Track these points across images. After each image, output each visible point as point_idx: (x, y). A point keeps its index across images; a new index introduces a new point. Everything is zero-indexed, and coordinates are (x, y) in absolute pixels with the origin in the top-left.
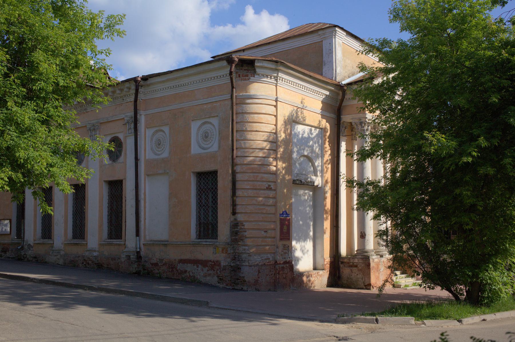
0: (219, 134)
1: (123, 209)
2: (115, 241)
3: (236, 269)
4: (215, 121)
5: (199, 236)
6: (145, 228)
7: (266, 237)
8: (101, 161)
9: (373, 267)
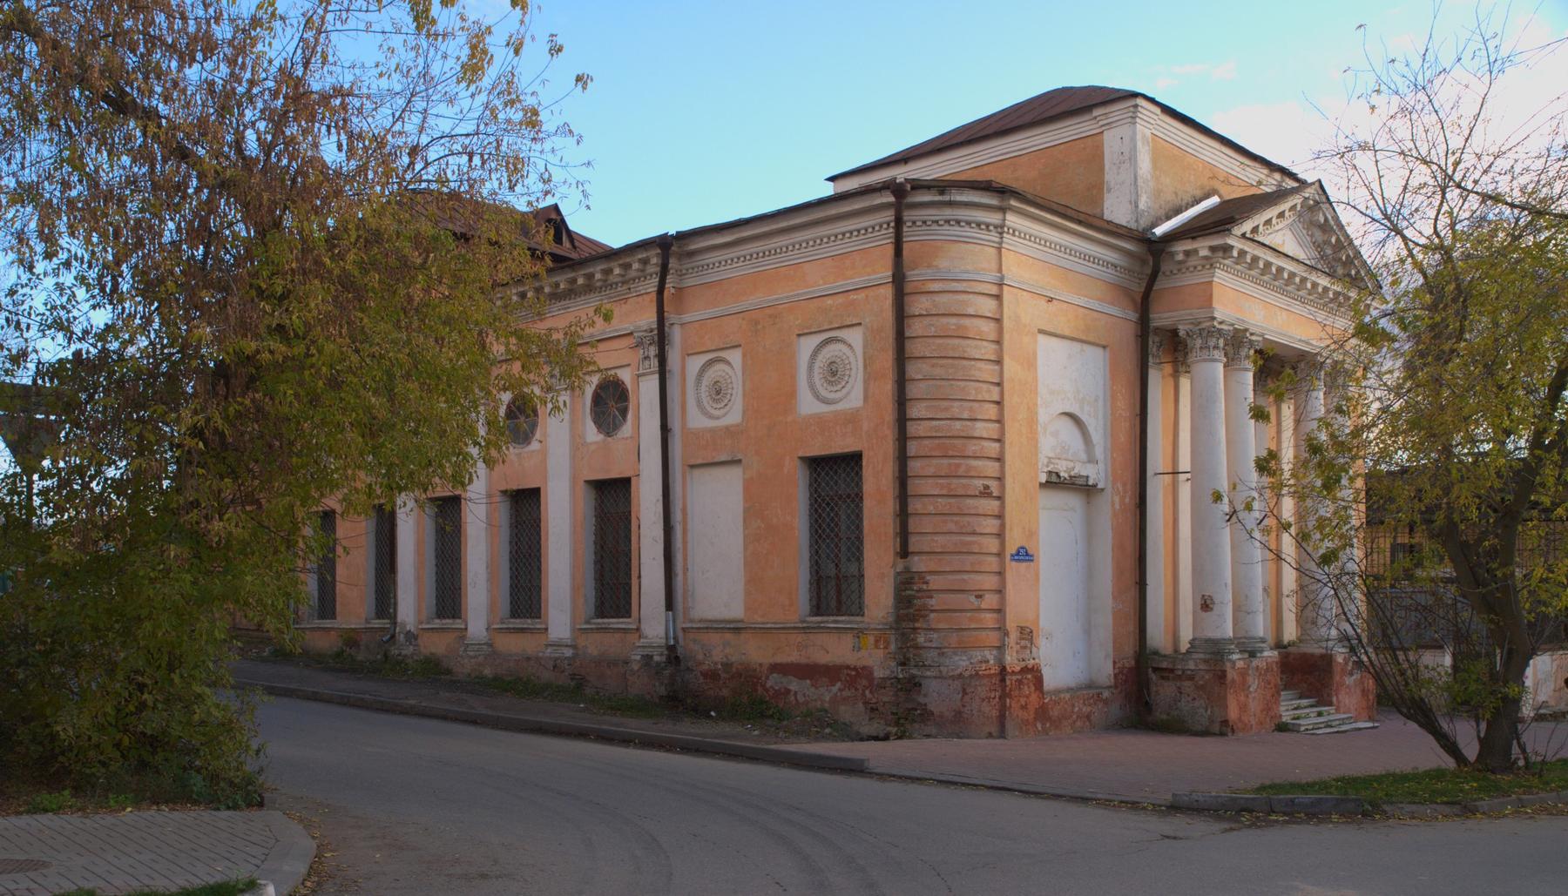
0: (865, 367)
2: (614, 622)
3: (912, 686)
4: (855, 337)
9: (1233, 681)
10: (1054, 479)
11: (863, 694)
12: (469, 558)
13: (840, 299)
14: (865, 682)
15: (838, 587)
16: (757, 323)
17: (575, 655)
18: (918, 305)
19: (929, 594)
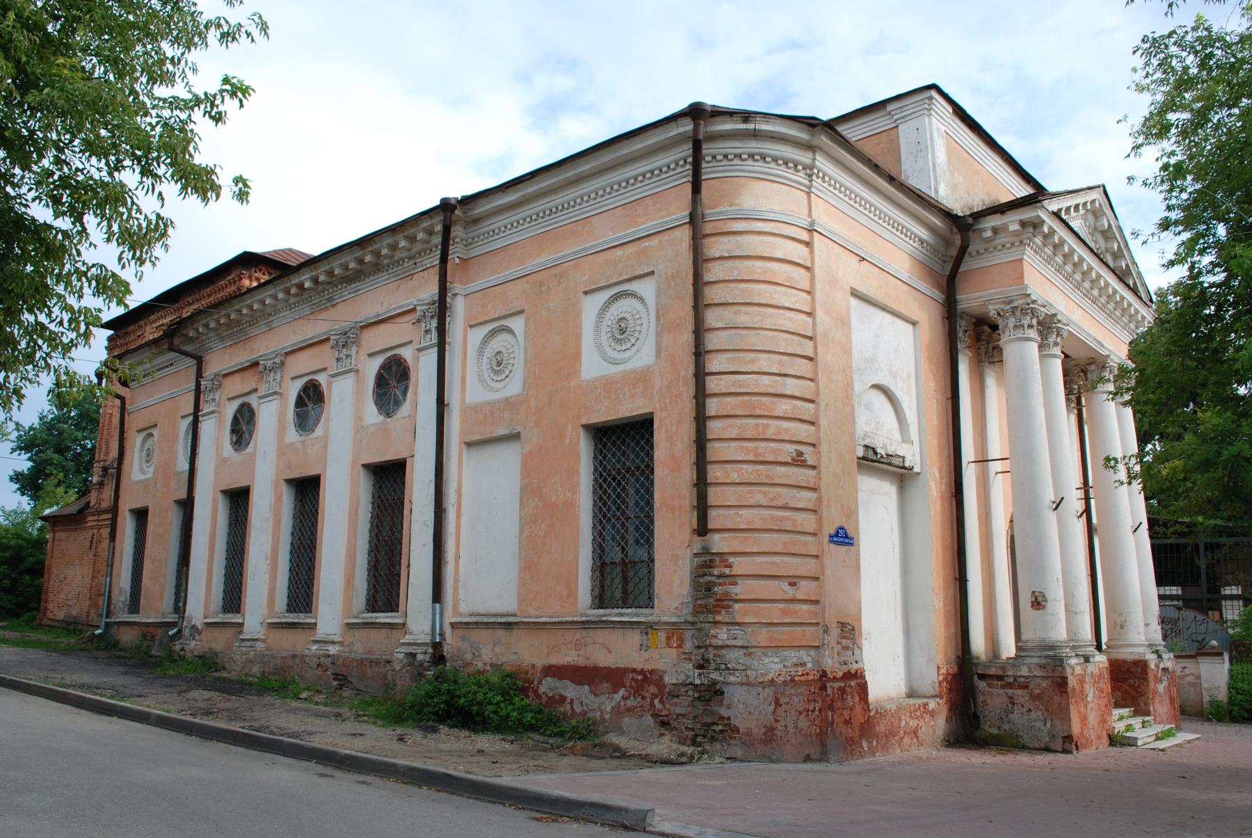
0: (658, 318)
1: (405, 532)
3: (713, 693)
4: (646, 288)
5: (601, 600)
6: (456, 581)
7: (794, 600)
8: (359, 418)
10: (871, 455)
11: (652, 705)
12: (251, 543)
13: (630, 249)
14: (653, 689)
15: (624, 573)
16: (541, 284)
17: (268, 649)
18: (715, 247)
19: (733, 579)
